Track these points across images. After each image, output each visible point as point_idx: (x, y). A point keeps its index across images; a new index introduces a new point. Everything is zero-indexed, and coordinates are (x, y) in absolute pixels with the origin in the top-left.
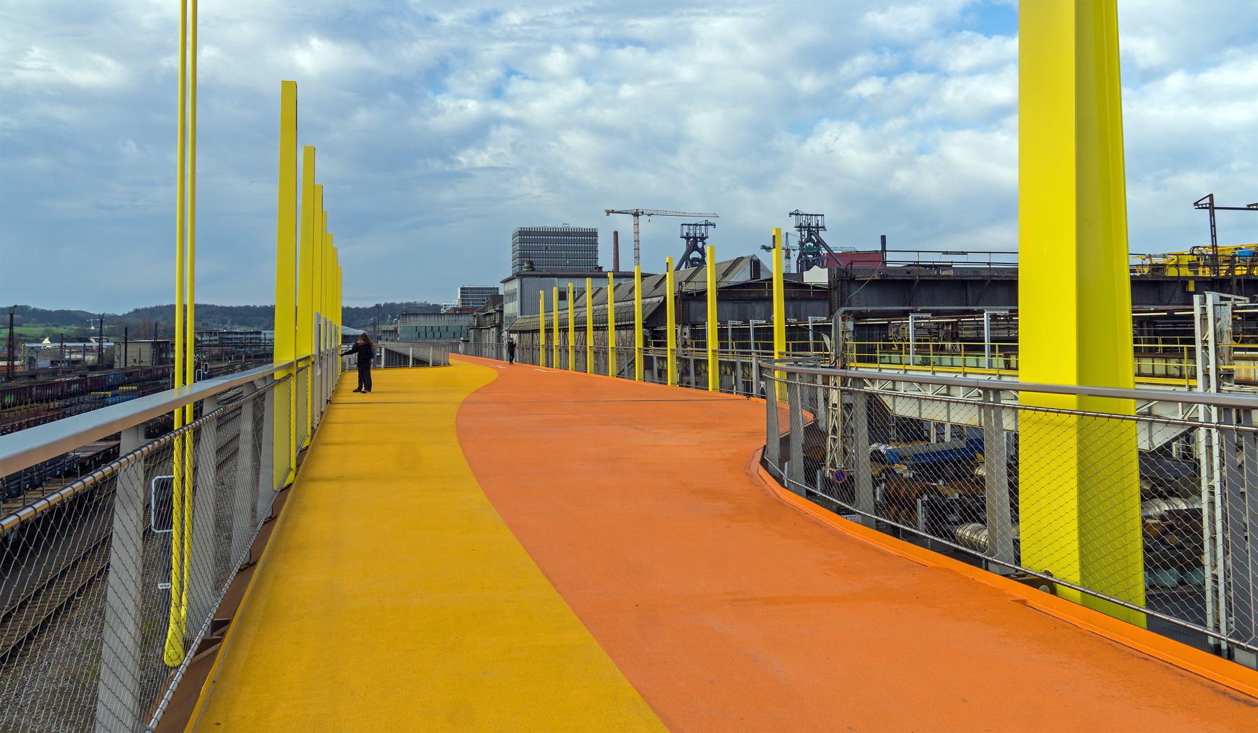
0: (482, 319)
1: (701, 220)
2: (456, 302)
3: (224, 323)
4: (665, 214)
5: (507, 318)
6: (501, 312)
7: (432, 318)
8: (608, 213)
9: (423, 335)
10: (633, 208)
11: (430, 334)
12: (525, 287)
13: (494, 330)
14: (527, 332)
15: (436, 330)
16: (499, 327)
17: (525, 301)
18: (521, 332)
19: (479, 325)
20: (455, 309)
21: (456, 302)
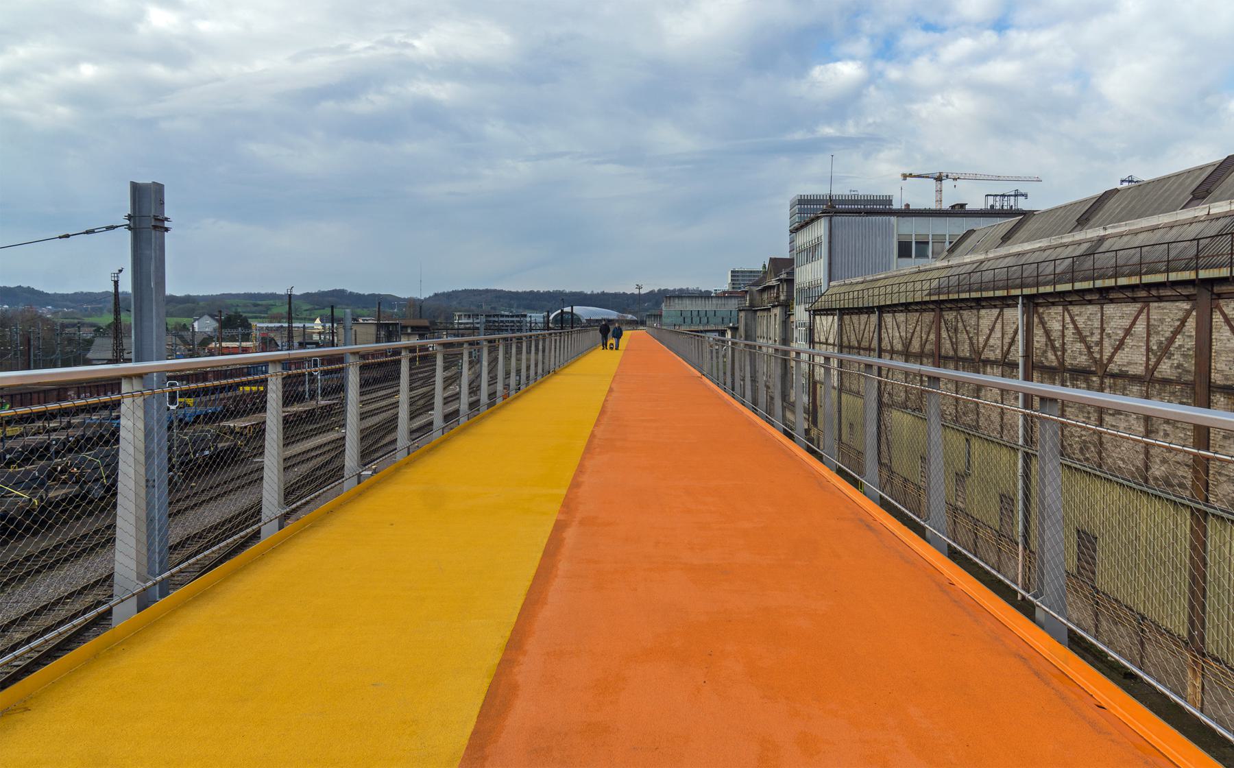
0: (758, 297)
1: (1009, 188)
2: (725, 285)
3: (511, 306)
4: (975, 178)
5: (801, 290)
6: (790, 282)
7: (699, 302)
8: (905, 177)
9: (688, 320)
10: (935, 169)
11: (696, 319)
12: (836, 232)
13: (777, 311)
14: (869, 310)
15: (702, 314)
16: (787, 307)
17: (837, 259)
18: (843, 312)
19: (752, 305)
20: (724, 292)
21: (725, 285)
